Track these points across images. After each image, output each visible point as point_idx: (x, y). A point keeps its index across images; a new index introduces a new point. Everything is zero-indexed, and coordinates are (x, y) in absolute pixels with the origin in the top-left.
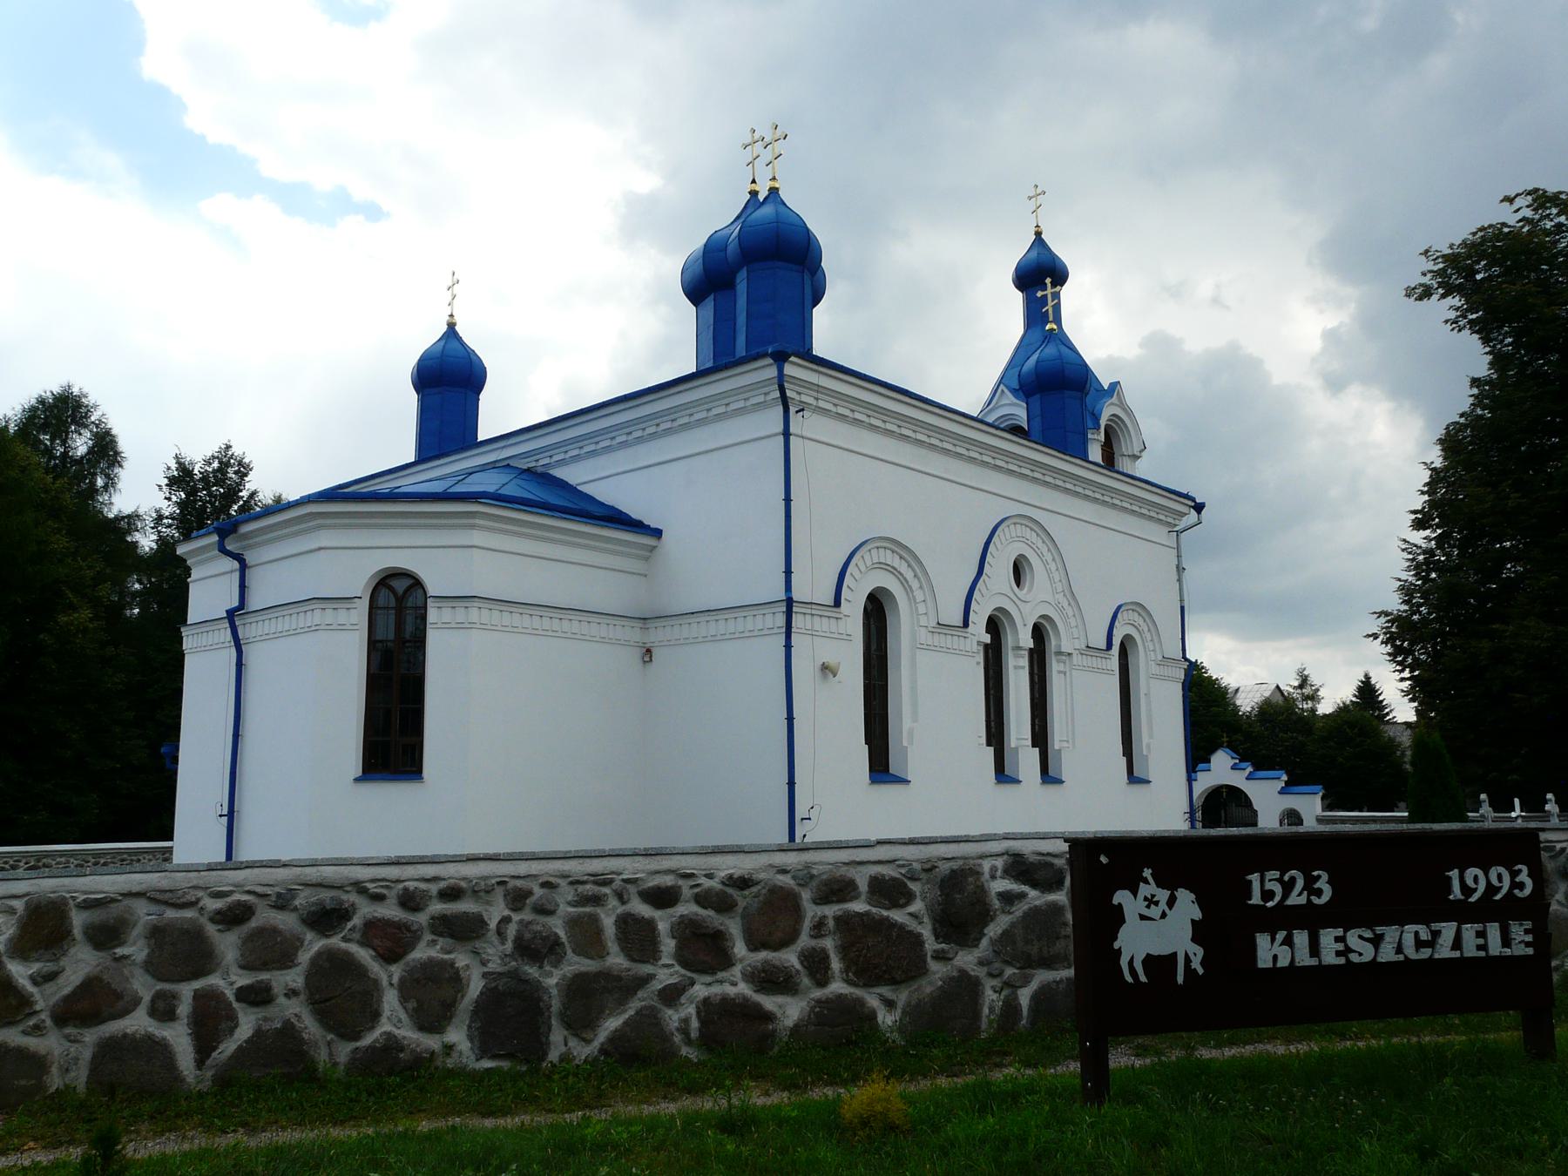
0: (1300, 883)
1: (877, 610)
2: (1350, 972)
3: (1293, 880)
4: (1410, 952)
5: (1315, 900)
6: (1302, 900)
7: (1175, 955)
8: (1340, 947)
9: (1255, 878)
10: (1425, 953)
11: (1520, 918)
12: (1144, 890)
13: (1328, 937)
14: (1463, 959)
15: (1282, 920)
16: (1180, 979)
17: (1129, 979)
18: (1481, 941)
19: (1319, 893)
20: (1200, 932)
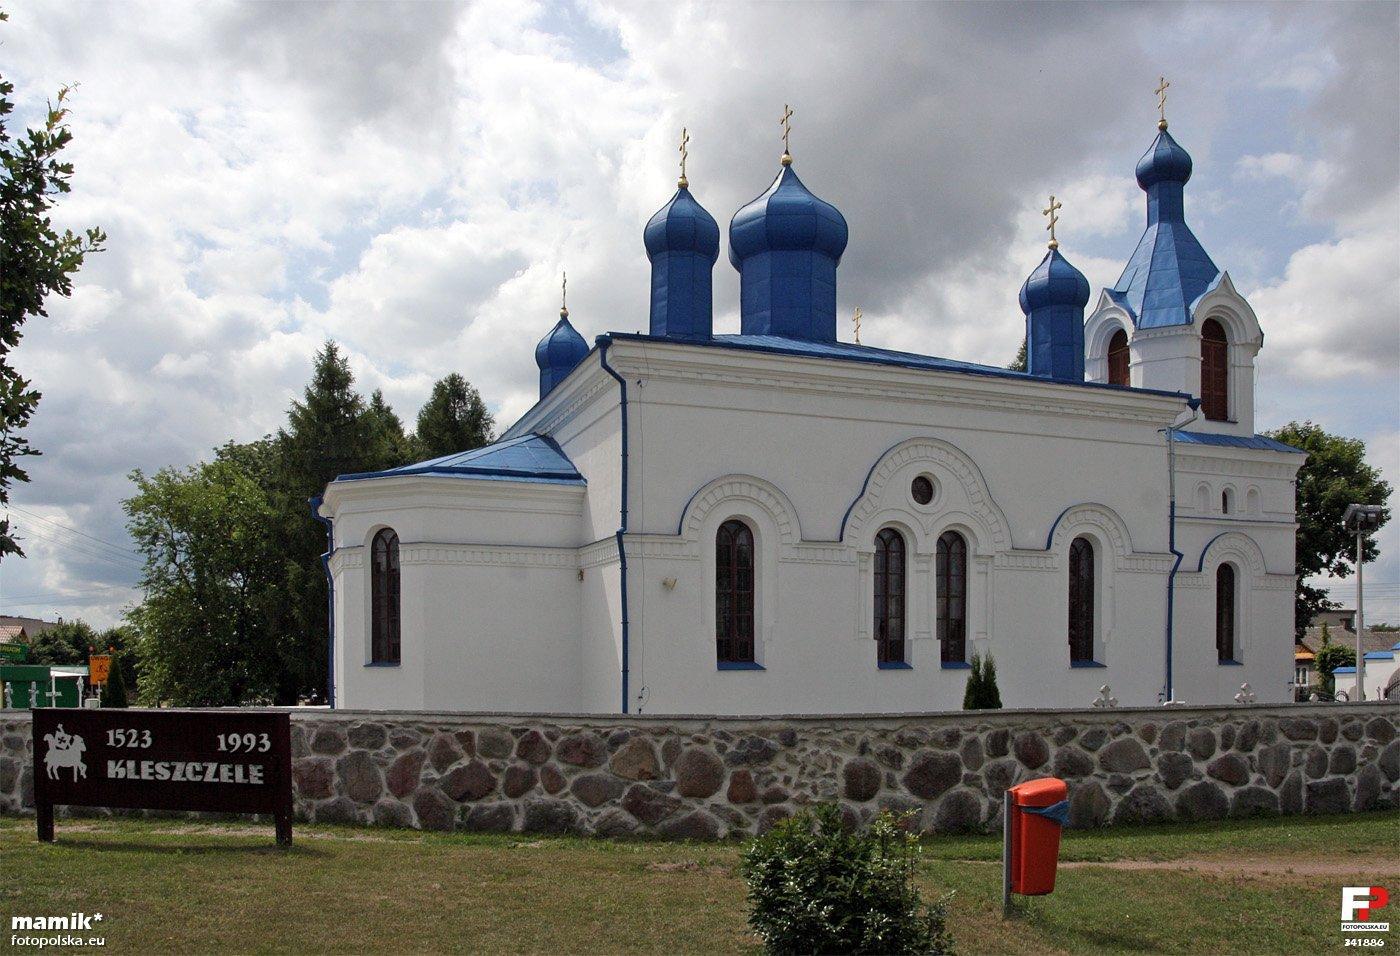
0: (134, 737)
1: (1226, 575)
2: (155, 784)
3: (131, 734)
4: (190, 776)
5: (143, 746)
6: (136, 745)
7: (72, 767)
8: (152, 771)
9: (111, 733)
10: (199, 778)
11: (255, 764)
12: (59, 734)
13: (145, 765)
14: (219, 783)
15: (122, 754)
16: (75, 780)
17: (51, 777)
18: (231, 774)
19: (145, 742)
20: (85, 757)
